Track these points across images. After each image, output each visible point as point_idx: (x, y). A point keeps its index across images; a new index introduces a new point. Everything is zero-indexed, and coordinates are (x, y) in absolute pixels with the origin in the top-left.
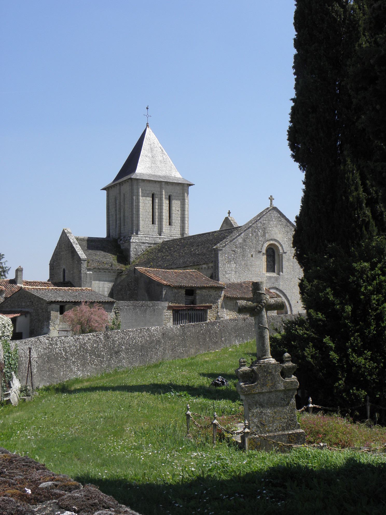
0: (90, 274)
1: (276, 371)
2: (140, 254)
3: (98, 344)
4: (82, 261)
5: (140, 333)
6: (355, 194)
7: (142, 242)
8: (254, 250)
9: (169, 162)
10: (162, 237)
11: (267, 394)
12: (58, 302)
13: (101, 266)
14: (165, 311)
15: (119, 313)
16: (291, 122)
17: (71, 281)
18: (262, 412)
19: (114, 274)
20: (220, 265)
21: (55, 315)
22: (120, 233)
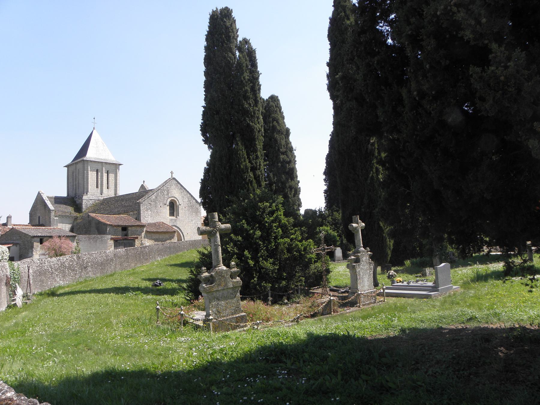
0: (56, 219)
1: (227, 275)
3: (73, 263)
5: (100, 254)
6: (244, 163)
8: (162, 203)
11: (221, 291)
12: (38, 236)
13: (64, 214)
14: (109, 241)
15: (79, 243)
16: (202, 120)
17: (44, 223)
18: (218, 304)
20: (141, 212)
21: (37, 245)
22: (76, 194)
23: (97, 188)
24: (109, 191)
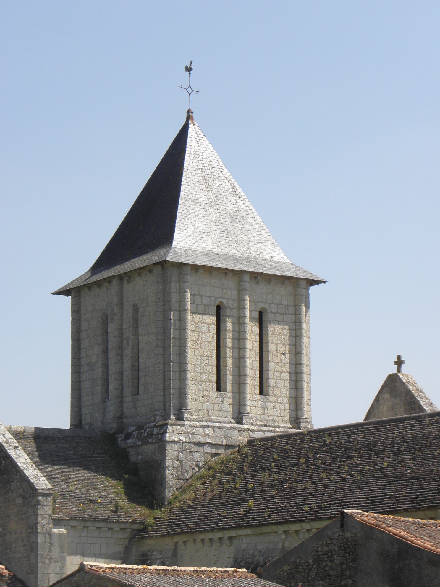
0: (60, 535)
2: (191, 477)
4: (40, 498)
7: (195, 441)
9: (254, 218)
10: (246, 427)
19: (120, 535)
22: (121, 417)
23: (218, 389)
24: (270, 405)
